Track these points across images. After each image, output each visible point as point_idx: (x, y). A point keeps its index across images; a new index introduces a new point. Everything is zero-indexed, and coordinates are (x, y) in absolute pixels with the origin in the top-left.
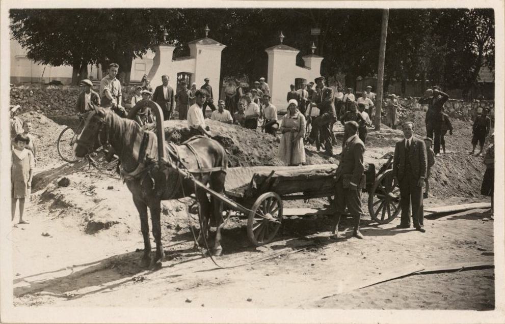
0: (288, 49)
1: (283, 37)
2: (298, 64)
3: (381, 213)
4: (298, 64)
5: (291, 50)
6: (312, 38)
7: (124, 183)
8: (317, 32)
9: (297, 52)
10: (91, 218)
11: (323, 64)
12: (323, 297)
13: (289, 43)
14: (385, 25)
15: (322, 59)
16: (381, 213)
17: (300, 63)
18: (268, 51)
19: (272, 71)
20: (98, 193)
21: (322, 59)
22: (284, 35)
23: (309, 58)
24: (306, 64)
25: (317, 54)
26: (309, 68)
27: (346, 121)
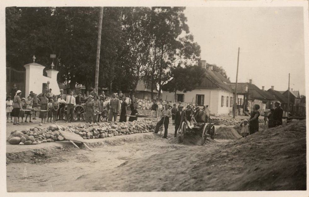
0: (38, 66)
1: (35, 58)
2: (44, 75)
3: (140, 65)
4: (44, 75)
5: (40, 66)
6: (51, 60)
7: (51, 89)
8: (54, 57)
9: (44, 67)
10: (192, 41)
11: (58, 75)
12: (77, 178)
13: (39, 62)
14: (98, 52)
15: (58, 72)
16: (140, 65)
17: (45, 74)
18: (25, 66)
19: (29, 76)
20: (37, 94)
21: (58, 72)
22: (35, 57)
23: (50, 72)
24: (48, 75)
25: (55, 69)
26: (50, 77)
27: (112, 84)
